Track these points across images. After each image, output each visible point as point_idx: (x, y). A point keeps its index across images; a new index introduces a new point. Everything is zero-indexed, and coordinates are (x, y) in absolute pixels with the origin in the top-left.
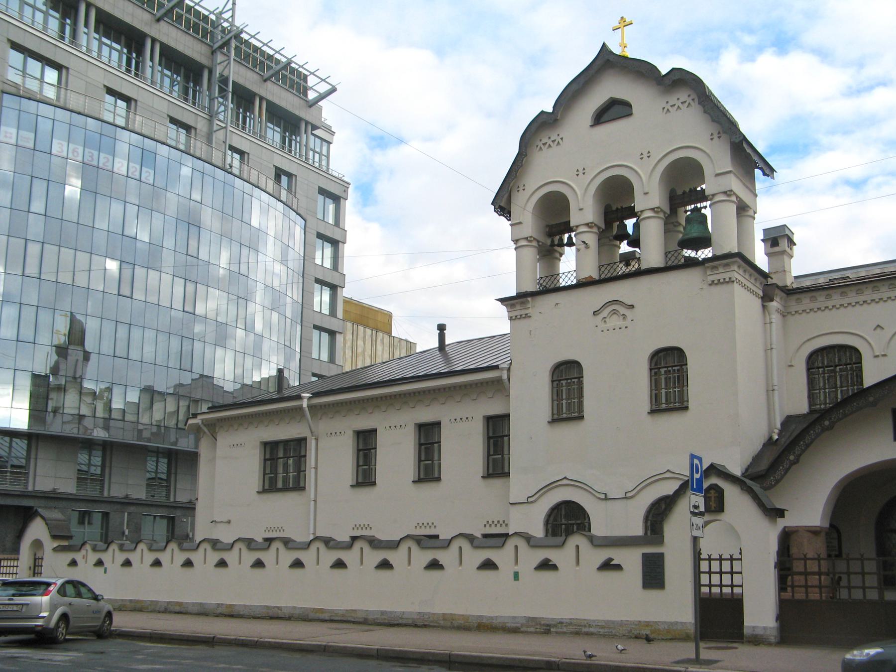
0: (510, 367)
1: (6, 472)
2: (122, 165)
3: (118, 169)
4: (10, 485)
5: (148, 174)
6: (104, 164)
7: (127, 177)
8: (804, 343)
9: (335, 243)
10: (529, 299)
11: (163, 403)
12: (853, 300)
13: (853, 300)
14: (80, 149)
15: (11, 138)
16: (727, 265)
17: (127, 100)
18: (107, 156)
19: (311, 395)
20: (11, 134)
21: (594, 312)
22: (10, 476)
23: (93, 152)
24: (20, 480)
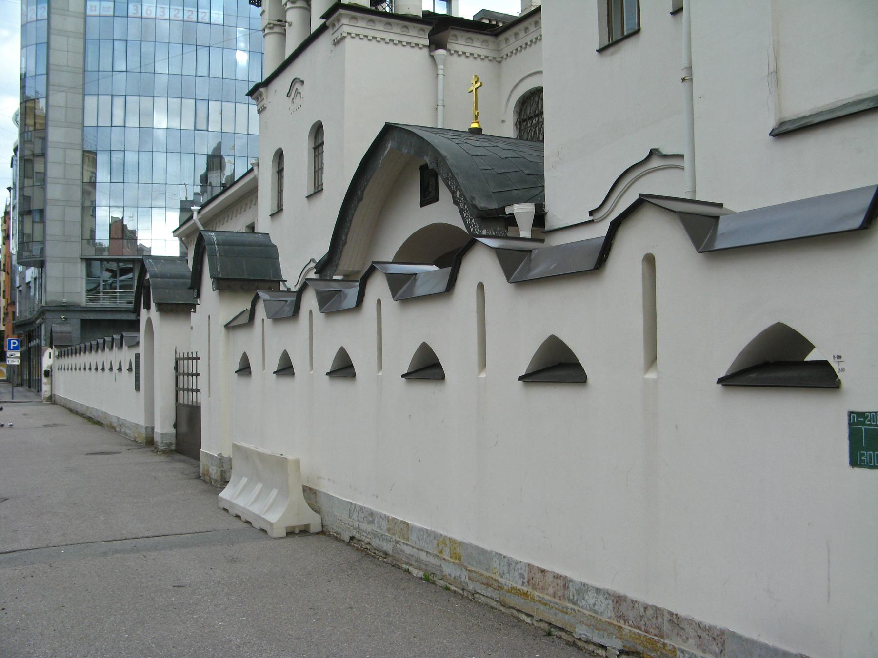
1: (99, 292)
3: (202, 19)
4: (120, 303)
6: (188, 17)
7: (197, 22)
8: (512, 91)
10: (262, 90)
11: (42, 225)
12: (396, 38)
13: (379, 35)
15: (95, 10)
16: (354, 18)
19: (200, 208)
20: (95, 7)
21: (287, 96)
22: (120, 296)
24: (116, 298)
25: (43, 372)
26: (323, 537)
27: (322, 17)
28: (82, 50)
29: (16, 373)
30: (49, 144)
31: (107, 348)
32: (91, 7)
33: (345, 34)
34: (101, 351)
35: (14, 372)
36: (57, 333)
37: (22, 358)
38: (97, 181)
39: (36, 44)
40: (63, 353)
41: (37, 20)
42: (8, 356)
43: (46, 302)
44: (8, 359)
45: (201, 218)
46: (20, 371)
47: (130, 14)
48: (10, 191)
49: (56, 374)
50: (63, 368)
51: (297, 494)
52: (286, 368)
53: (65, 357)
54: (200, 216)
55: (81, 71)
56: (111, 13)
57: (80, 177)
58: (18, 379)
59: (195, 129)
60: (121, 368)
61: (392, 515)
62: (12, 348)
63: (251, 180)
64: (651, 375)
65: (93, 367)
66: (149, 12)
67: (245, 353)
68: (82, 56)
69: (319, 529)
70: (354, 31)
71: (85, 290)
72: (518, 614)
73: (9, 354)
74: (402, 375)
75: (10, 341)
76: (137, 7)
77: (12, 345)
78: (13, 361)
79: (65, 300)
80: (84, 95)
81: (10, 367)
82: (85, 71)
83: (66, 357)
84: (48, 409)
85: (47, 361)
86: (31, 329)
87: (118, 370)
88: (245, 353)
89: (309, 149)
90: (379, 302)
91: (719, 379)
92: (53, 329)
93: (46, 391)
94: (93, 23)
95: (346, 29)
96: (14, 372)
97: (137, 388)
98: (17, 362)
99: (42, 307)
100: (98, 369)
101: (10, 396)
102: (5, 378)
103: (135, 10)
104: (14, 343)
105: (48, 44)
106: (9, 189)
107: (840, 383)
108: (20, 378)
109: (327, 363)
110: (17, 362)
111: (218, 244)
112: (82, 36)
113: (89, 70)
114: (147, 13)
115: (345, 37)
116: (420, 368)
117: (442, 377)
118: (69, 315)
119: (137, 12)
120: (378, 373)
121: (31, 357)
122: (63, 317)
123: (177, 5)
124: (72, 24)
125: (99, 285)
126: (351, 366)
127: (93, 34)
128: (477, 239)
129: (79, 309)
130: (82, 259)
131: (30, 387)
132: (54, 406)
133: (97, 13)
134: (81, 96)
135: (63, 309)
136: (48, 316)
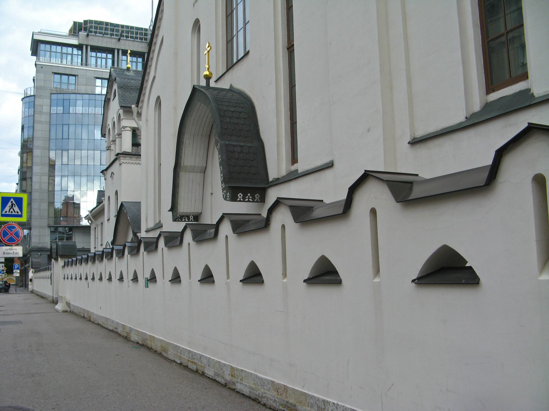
0: (91, 321)
2: (99, 110)
5: (98, 110)
9: (220, 121)
10: (105, 172)
13: (134, 162)
14: (87, 108)
17: (75, 76)
18: (73, 107)
23: (92, 108)
25: (29, 280)
26: (70, 313)
27: (116, 156)
28: (48, 130)
29: (20, 281)
30: (33, 174)
31: (79, 264)
32: (53, 109)
33: (122, 163)
34: (74, 266)
35: (19, 280)
36: (35, 262)
37: (21, 273)
38: (55, 190)
39: (28, 127)
40: (46, 269)
41: (29, 116)
42: (14, 272)
43: (32, 248)
44: (14, 274)
45: (92, 214)
46: (22, 279)
47: (71, 112)
48: (17, 185)
49: (34, 280)
50: (48, 277)
51: (65, 303)
52: (176, 278)
53: (48, 270)
54: (91, 214)
55: (48, 139)
56: (62, 112)
57: (47, 188)
58: (21, 283)
59: (101, 165)
60: (102, 278)
61: (106, 317)
62: (16, 268)
63: (102, 206)
64: (377, 280)
65: (70, 277)
66: (79, 111)
67: (153, 269)
68: (48, 133)
69: (70, 311)
70: (124, 161)
71: (49, 241)
72: (270, 401)
73: (14, 271)
74: (240, 280)
75: (15, 265)
76: (74, 109)
77: (16, 267)
78: (16, 275)
79: (40, 246)
80: (49, 150)
81: (17, 277)
82: (50, 139)
83: (48, 271)
84: (30, 296)
85: (31, 275)
86: (26, 258)
87: (85, 279)
88: (153, 269)
89: (115, 199)
90: (283, 227)
91: (304, 280)
92: (33, 261)
93: (30, 288)
94: (54, 117)
95: (122, 161)
96: (19, 280)
97: (51, 284)
98: (18, 275)
99: (30, 249)
100: (73, 278)
101: (15, 291)
102: (14, 283)
103: (73, 110)
104: (17, 266)
105: (33, 127)
106: (17, 184)
107: (341, 281)
108: (22, 283)
109: (240, 272)
110: (18, 275)
111: (61, 246)
112: (49, 123)
113: (52, 138)
114: (78, 112)
115: (121, 164)
116: (316, 275)
117: (339, 282)
118: (42, 253)
119: (74, 111)
120: (227, 280)
121: (24, 273)
122: (39, 254)
123: (92, 107)
124: (44, 118)
125: (56, 238)
126: (212, 276)
127: (53, 122)
128: (280, 200)
129: (47, 250)
130: (48, 227)
131: (25, 287)
132: (33, 294)
133: (55, 112)
134: (48, 151)
135: (39, 250)
136: (32, 253)
